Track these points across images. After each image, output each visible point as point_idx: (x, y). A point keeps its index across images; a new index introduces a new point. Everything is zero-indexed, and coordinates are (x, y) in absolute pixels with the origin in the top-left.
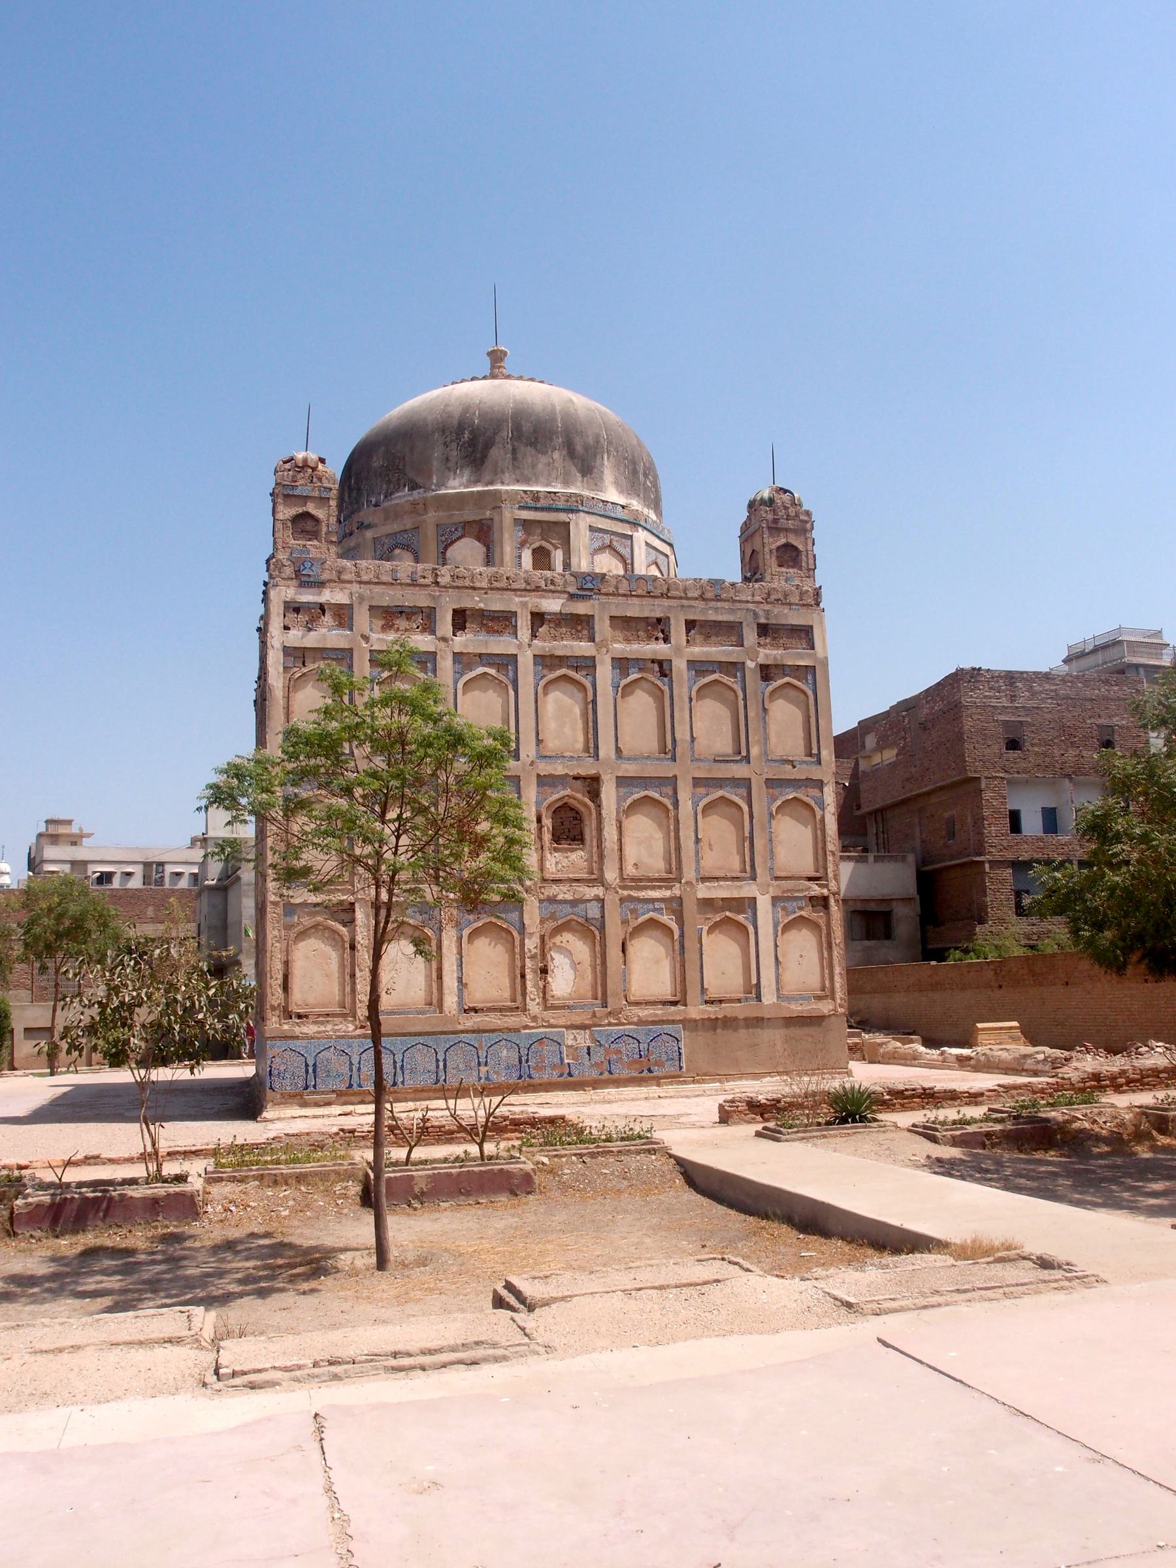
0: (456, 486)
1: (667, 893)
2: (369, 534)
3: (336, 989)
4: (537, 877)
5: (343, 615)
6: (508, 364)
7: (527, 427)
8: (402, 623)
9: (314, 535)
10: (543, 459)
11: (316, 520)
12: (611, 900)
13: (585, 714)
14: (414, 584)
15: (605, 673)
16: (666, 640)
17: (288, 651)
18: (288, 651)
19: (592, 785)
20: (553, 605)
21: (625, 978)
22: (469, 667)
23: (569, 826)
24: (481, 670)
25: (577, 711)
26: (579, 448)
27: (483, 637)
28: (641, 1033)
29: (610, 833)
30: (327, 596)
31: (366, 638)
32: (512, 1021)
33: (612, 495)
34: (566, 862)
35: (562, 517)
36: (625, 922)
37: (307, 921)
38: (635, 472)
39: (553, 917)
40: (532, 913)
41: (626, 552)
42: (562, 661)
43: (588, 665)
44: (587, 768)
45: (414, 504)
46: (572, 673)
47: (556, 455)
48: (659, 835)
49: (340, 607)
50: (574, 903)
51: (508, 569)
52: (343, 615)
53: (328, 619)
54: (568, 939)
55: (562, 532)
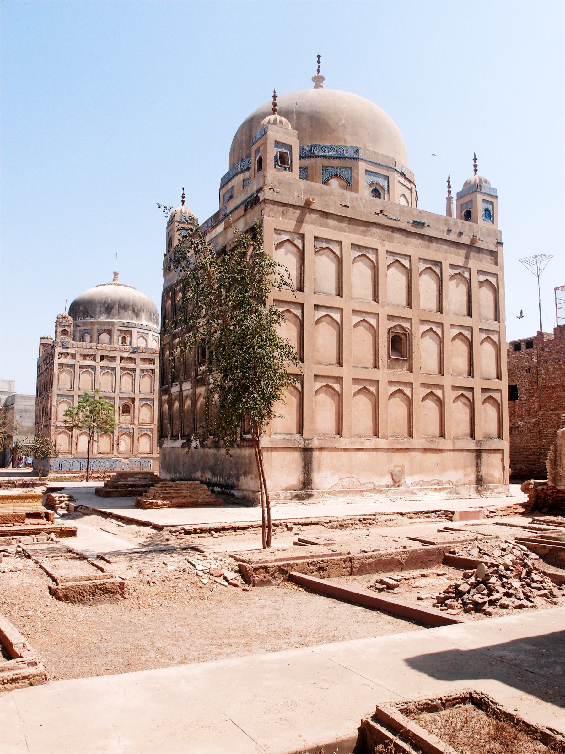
0: (103, 319)
1: (150, 427)
2: (78, 328)
3: (67, 447)
4: (118, 422)
5: (73, 356)
6: (120, 280)
7: (122, 304)
8: (88, 358)
9: (67, 335)
10: (126, 313)
11: (67, 331)
12: (136, 428)
13: (132, 383)
14: (91, 348)
15: (138, 372)
16: (154, 364)
17: (59, 364)
18: (59, 364)
19: (133, 400)
20: (126, 355)
21: (138, 447)
22: (104, 370)
23: (126, 410)
24: (107, 371)
25: (130, 381)
26: (136, 310)
27: (108, 362)
28: (141, 460)
29: (137, 412)
30: (69, 351)
31: (79, 362)
32: (110, 456)
33: (144, 322)
34: (126, 418)
35: (130, 329)
36: (139, 433)
37: (61, 430)
38: (151, 315)
39: (121, 432)
40: (116, 432)
41: (146, 338)
42: (127, 369)
43: (134, 370)
44: (132, 396)
45: (91, 322)
46: (129, 372)
47: (130, 312)
48: (149, 413)
49: (73, 354)
50: (127, 428)
51: (115, 345)
52: (73, 356)
53: (69, 356)
54: (125, 437)
55: (130, 332)
